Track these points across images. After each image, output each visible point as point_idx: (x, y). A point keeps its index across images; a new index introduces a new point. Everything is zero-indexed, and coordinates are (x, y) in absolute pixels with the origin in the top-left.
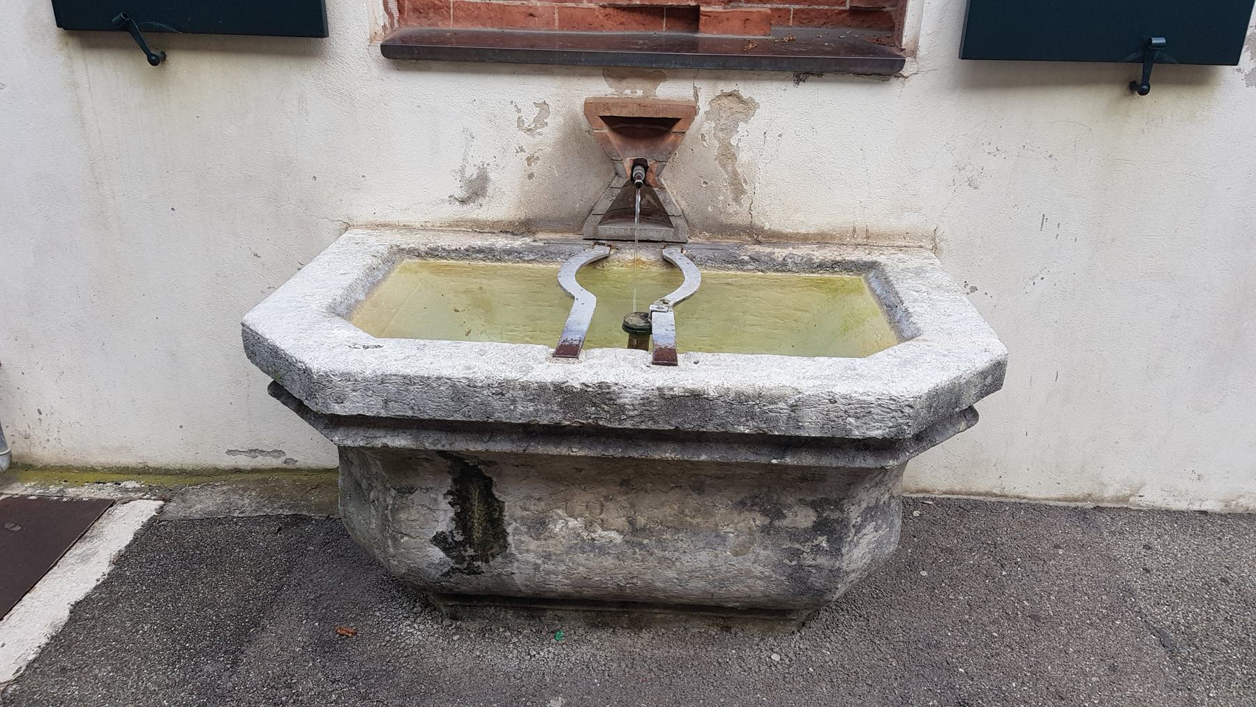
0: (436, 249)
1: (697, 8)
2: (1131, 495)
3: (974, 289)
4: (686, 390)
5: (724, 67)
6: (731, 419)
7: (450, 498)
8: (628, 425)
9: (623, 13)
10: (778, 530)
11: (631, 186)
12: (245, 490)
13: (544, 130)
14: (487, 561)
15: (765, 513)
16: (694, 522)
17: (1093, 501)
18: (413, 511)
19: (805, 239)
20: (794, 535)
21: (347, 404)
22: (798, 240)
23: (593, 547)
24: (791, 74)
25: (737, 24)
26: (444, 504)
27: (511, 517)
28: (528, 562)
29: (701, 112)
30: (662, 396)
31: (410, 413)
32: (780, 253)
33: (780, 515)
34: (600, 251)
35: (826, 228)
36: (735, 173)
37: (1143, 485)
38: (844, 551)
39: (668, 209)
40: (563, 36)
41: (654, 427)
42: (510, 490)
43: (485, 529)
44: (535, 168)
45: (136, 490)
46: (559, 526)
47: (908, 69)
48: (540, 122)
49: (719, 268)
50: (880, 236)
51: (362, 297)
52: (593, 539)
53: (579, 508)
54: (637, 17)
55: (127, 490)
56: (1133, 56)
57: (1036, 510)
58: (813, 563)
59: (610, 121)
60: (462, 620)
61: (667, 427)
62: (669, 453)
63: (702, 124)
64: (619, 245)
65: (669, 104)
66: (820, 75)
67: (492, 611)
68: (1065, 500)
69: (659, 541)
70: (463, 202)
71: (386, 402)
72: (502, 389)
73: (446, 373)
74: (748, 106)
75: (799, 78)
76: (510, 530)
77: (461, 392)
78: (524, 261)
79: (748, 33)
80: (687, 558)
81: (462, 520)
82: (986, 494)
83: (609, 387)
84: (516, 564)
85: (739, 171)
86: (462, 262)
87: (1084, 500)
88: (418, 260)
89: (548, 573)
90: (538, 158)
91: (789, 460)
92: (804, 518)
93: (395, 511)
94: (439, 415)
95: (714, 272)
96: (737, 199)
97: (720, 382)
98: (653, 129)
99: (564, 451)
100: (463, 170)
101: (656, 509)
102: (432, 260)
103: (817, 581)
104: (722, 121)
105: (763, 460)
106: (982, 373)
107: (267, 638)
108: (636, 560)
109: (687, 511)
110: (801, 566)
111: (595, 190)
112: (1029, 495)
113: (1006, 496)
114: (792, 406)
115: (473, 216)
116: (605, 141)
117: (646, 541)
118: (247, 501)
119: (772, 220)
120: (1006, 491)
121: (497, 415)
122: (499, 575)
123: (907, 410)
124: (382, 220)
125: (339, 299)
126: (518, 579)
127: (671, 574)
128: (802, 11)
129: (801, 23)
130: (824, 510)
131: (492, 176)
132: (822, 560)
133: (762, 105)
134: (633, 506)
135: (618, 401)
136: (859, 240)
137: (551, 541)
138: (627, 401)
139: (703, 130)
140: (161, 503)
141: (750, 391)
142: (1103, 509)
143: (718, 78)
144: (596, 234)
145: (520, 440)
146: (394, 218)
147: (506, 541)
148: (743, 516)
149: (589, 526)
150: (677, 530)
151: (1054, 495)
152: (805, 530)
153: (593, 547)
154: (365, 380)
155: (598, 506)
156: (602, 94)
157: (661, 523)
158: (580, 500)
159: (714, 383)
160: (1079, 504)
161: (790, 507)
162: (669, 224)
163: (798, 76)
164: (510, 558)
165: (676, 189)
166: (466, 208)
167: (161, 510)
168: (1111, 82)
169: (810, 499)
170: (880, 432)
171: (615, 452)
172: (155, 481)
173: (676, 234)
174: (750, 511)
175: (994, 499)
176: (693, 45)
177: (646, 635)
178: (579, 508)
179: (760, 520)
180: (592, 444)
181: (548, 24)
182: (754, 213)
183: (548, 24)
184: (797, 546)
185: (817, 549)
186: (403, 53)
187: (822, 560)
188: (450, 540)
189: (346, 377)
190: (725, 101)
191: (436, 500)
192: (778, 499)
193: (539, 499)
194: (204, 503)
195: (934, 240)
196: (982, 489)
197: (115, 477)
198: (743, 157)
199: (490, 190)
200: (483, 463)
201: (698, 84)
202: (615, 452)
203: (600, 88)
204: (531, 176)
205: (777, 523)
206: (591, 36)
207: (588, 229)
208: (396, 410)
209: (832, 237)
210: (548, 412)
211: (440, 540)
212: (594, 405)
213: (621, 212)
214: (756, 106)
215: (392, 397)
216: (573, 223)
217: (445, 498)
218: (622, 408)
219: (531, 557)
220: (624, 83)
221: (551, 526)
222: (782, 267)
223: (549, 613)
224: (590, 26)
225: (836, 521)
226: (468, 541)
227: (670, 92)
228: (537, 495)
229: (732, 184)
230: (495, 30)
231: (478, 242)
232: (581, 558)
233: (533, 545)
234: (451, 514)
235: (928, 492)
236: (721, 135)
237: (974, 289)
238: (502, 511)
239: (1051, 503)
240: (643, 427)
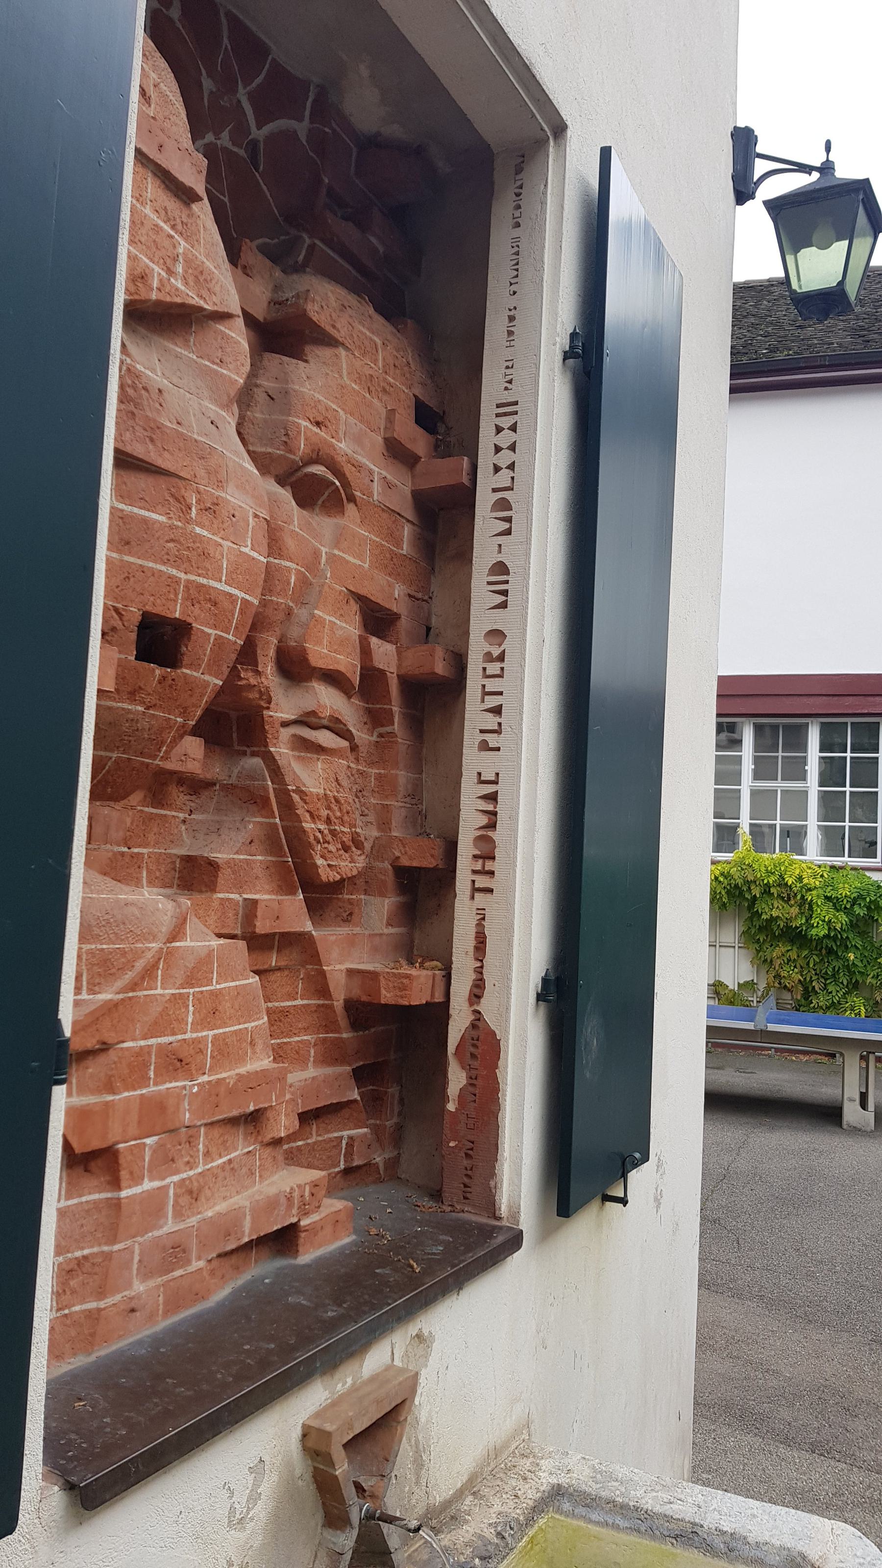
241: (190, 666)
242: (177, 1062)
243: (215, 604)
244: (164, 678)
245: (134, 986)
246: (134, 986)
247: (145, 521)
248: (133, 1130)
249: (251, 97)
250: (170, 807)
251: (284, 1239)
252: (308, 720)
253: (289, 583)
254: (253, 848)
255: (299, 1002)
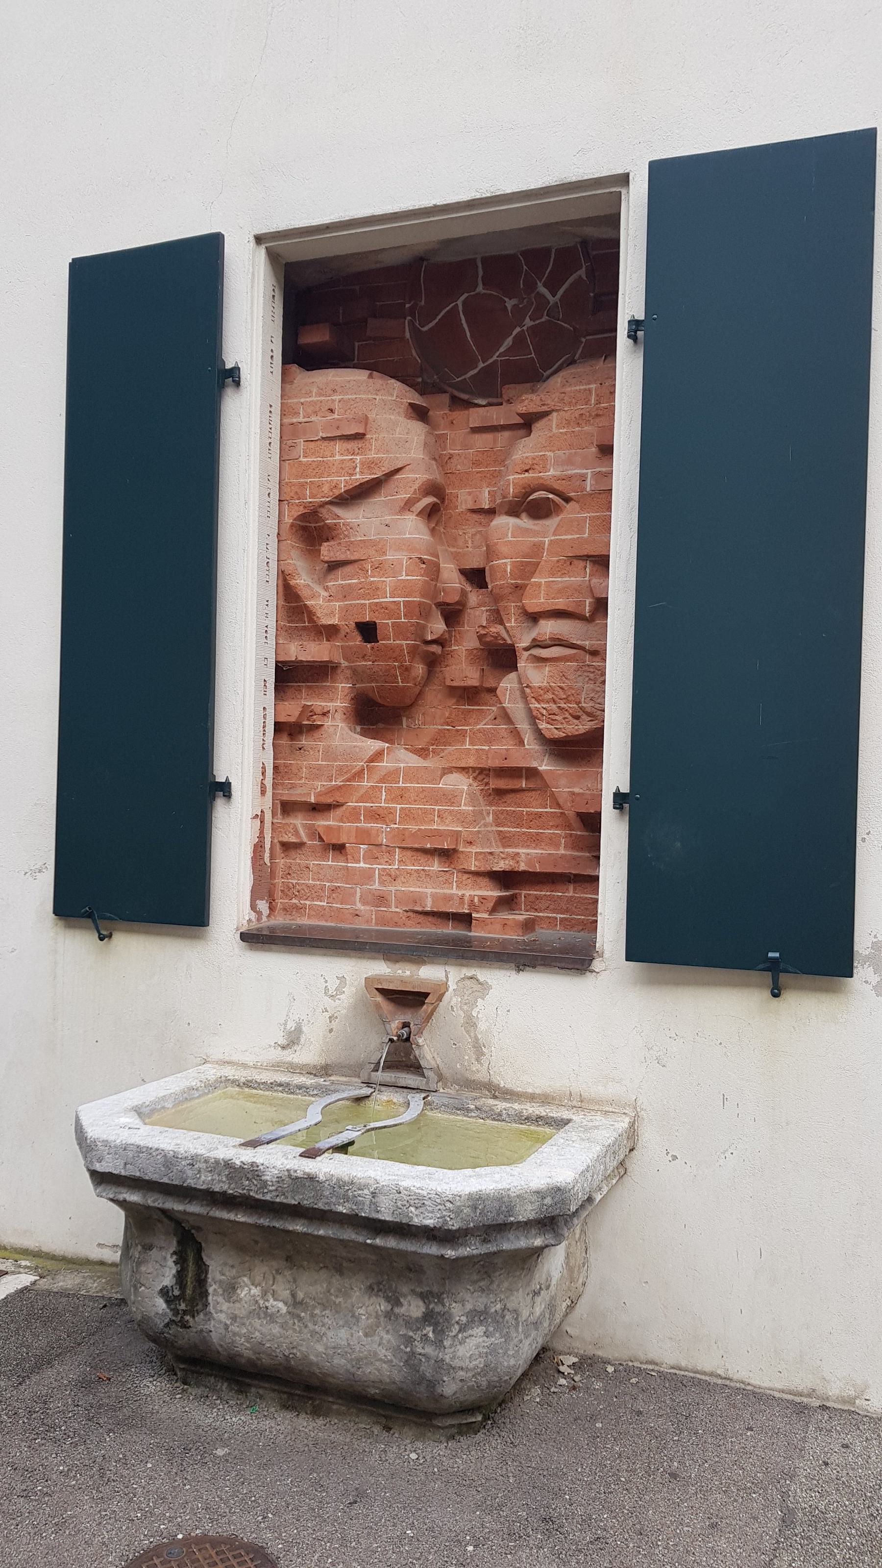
0: (251, 1081)
1: (470, 915)
2: (856, 1397)
3: (675, 1158)
4: (305, 1173)
5: (463, 958)
6: (334, 1200)
7: (175, 1257)
8: (268, 1197)
9: (419, 916)
10: (397, 1316)
11: (400, 1045)
12: (99, 1277)
13: (342, 997)
14: (193, 1317)
15: (388, 1299)
16: (338, 1300)
17: (818, 1398)
18: (150, 1266)
19: (532, 1098)
20: (408, 1323)
21: (103, 1163)
22: (527, 1098)
23: (266, 1313)
24: (513, 965)
25: (498, 927)
26: (170, 1262)
27: (213, 1279)
28: (220, 1322)
29: (451, 989)
30: (290, 1176)
31: (138, 1174)
32: (500, 1105)
33: (397, 1303)
34: (366, 1091)
35: (548, 1090)
36: (476, 1039)
37: (867, 1387)
38: (447, 1343)
39: (423, 1063)
40: (377, 931)
41: (285, 1201)
42: (213, 1256)
43: (194, 1287)
44: (334, 1025)
45: (26, 1267)
46: (244, 1293)
47: (597, 965)
48: (339, 990)
49: (451, 1114)
50: (591, 1101)
51: (170, 1106)
52: (267, 1308)
53: (258, 1278)
54: (430, 919)
55: (20, 1266)
56: (761, 966)
57: (757, 1397)
58: (423, 1351)
59: (383, 992)
60: (189, 1385)
61: (293, 1202)
62: (299, 1227)
63: (451, 998)
64: (383, 1088)
65: (423, 982)
66: (534, 967)
67: (212, 1380)
68: (790, 1393)
69: (312, 1316)
70: (283, 1048)
71: (125, 1164)
72: (193, 1160)
73: (162, 1146)
74: (485, 987)
75: (519, 970)
76: (211, 1290)
77: (170, 1161)
78: (310, 1095)
79: (506, 934)
80: (330, 1334)
81: (180, 1277)
82: (711, 1374)
83: (258, 1166)
84: (213, 1322)
85: (479, 1037)
86: (267, 1093)
87: (809, 1396)
88: (237, 1089)
89: (235, 1334)
90: (336, 1017)
91: (378, 1241)
92: (414, 1308)
93: (139, 1263)
94: (155, 1177)
95: (446, 1116)
96: (478, 1060)
97: (328, 1170)
98: (410, 999)
99: (231, 1216)
100: (285, 1024)
101: (313, 1284)
102: (247, 1090)
103: (427, 1370)
104: (466, 998)
105: (361, 1239)
106: (537, 1192)
107: (50, 1372)
108: (295, 1330)
109: (332, 1291)
110: (413, 1353)
111: (375, 1046)
112: (752, 1382)
113: (731, 1380)
114: (372, 1193)
115: (289, 1059)
116: (378, 1006)
117: (303, 1314)
118: (95, 1285)
119: (506, 1081)
120: (730, 1374)
121: (189, 1181)
122: (202, 1331)
123: (448, 1205)
124: (227, 1059)
125: (147, 1103)
126: (215, 1338)
127: (320, 1348)
128: (566, 919)
129: (565, 928)
130: (430, 1302)
131: (304, 1029)
132: (429, 1350)
133: (493, 987)
134: (295, 1281)
135: (263, 1178)
136: (575, 1103)
137: (237, 1305)
138: (268, 1178)
139: (452, 1003)
140: (38, 1278)
141: (346, 1179)
142: (828, 1408)
143: (462, 965)
144: (369, 1079)
145: (207, 1205)
146: (234, 1058)
147: (207, 1300)
148: (372, 1300)
149: (264, 1293)
150: (325, 1308)
151: (779, 1386)
152: (417, 1319)
153: (266, 1313)
154: (115, 1147)
155: (271, 1278)
156: (382, 972)
157: (314, 1299)
158: (261, 1269)
159: (324, 1170)
160: (805, 1400)
161: (405, 1296)
162: (423, 1075)
163: (518, 967)
164: (209, 1316)
165: (428, 1049)
166: (286, 1052)
167: (34, 1283)
168: (760, 986)
169: (418, 1290)
170: (432, 1221)
171: (264, 1221)
172: (40, 1262)
173: (427, 1083)
174: (377, 1296)
175: (719, 1381)
176: (468, 941)
177: (320, 1421)
178: (258, 1278)
179: (384, 1306)
180: (251, 1214)
181: (367, 921)
182: (492, 1073)
183: (367, 921)
184: (411, 1334)
185: (425, 1338)
186: (253, 939)
187: (429, 1350)
188: (170, 1294)
189: (106, 1143)
190: (468, 982)
191: (165, 1258)
192: (396, 1287)
193: (233, 1266)
194: (67, 1281)
195: (635, 1108)
196: (708, 1368)
197: (17, 1256)
198: (482, 1026)
199: (302, 1040)
200: (194, 1227)
201: (448, 968)
202: (264, 1221)
203: (380, 969)
204: (331, 1031)
205: (397, 1310)
206: (398, 931)
207: (364, 1076)
208: (132, 1171)
209: (553, 1098)
210: (220, 1181)
211: (164, 1292)
212: (248, 1179)
213: (391, 1065)
214: (490, 987)
215: (130, 1161)
216: (352, 1070)
217: (171, 1257)
218: (265, 1184)
219: (222, 1317)
220: (398, 965)
221: (239, 1291)
222: (498, 1117)
223: (253, 1390)
224: (396, 924)
225: (439, 1313)
226: (181, 1297)
227: (428, 974)
228: (231, 1262)
229: (474, 1047)
230: (332, 924)
231: (283, 1078)
232: (257, 1323)
233: (225, 1306)
234: (174, 1271)
235: (657, 1364)
236: (465, 1007)
237: (675, 1158)
238: (207, 1273)
239: (777, 1395)
240: (278, 1200)
241: (383, 639)
242: (376, 816)
243: (387, 609)
244: (373, 648)
245: (349, 780)
246: (349, 780)
247: (349, 584)
248: (353, 840)
249: (545, 285)
250: (486, 704)
251: (466, 920)
252: (536, 644)
253: (506, 571)
254: (497, 721)
255: (548, 810)
